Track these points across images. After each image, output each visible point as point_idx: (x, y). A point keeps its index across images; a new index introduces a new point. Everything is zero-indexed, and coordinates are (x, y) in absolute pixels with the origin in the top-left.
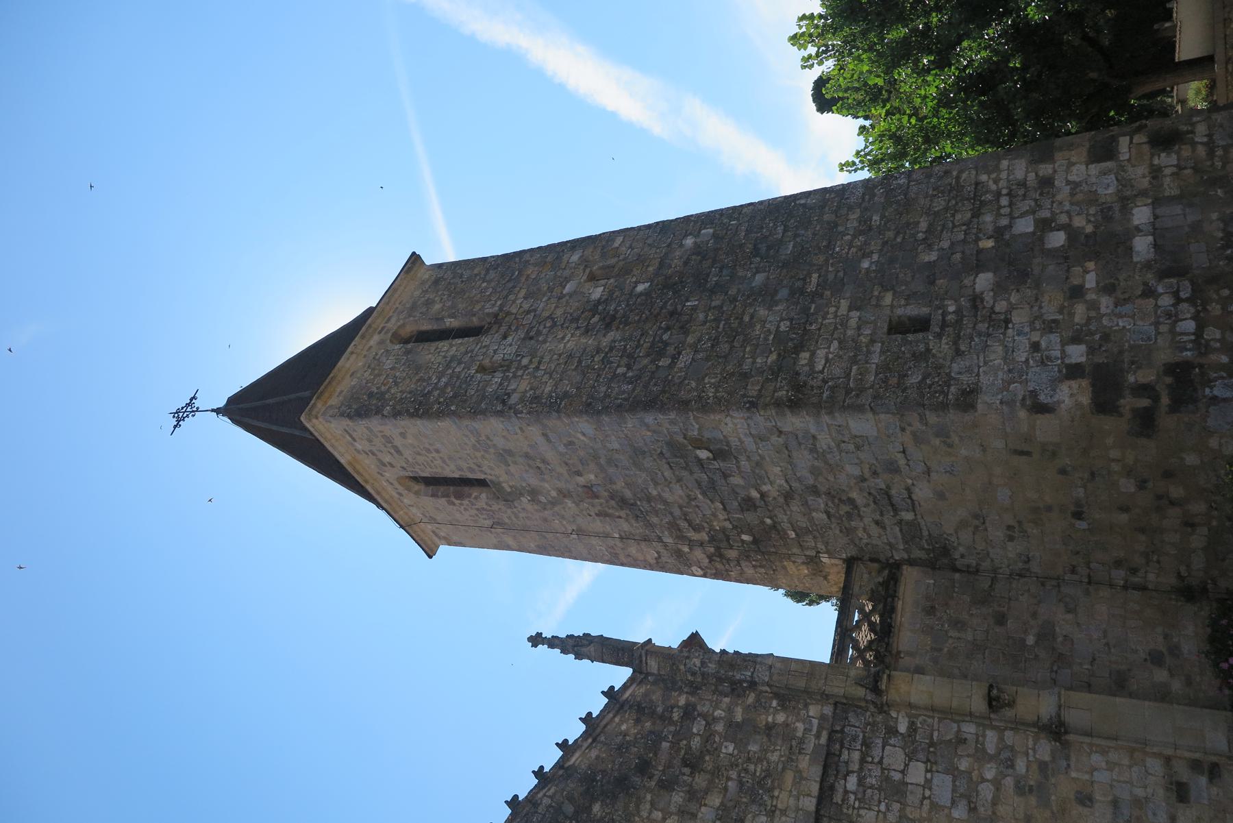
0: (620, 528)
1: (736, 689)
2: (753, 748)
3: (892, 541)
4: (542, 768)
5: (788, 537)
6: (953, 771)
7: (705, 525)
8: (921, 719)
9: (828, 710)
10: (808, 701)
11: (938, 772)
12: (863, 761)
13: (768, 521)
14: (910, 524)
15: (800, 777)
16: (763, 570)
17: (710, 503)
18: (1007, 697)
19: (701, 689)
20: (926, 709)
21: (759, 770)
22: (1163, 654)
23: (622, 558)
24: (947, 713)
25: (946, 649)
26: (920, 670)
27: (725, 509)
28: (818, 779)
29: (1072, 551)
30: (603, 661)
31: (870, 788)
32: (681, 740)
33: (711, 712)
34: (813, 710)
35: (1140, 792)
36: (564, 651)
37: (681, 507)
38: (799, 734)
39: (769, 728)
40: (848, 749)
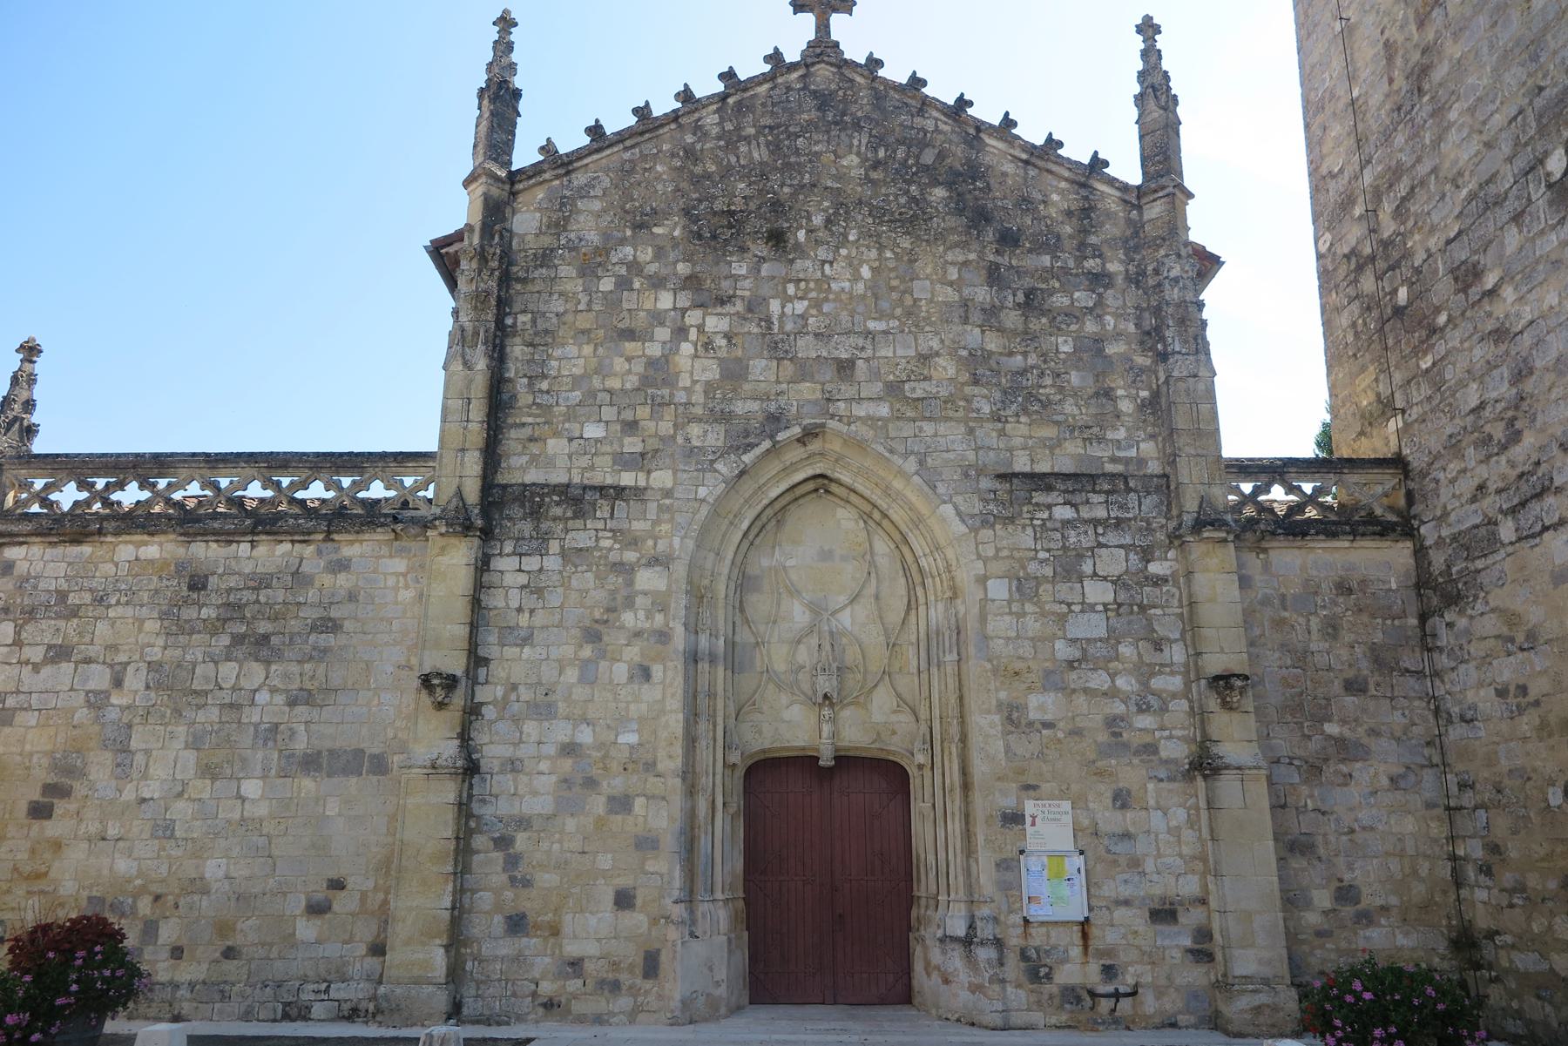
0: (1371, 92)
1: (1151, 338)
2: (1075, 378)
3: (1453, 517)
4: (970, 104)
5: (1418, 359)
6: (1113, 638)
7: (1410, 223)
8: (1174, 590)
9: (1154, 467)
10: (1160, 439)
11: (1108, 619)
12: (1096, 522)
13: (1442, 319)
14: (1493, 542)
15: (1053, 446)
16: (1350, 338)
17: (1456, 212)
18: (1235, 699)
19: (1138, 287)
20: (1190, 595)
21: (1047, 390)
22: (1357, 904)
23: (1320, 119)
24: (1191, 625)
25: (1286, 614)
26: (1244, 582)
27: (1449, 242)
28: (1056, 470)
29: (1500, 782)
30: (1141, 137)
31: (1063, 536)
32: (1058, 280)
33: (1109, 310)
34: (1148, 448)
35: (1149, 866)
36: (1142, 76)
37: (1435, 170)
38: (1110, 435)
39: (1108, 394)
40: (1107, 502)
